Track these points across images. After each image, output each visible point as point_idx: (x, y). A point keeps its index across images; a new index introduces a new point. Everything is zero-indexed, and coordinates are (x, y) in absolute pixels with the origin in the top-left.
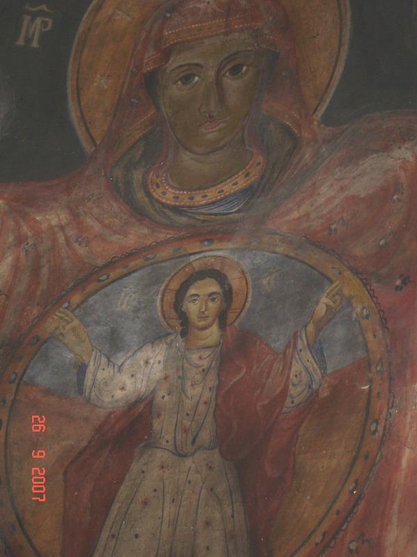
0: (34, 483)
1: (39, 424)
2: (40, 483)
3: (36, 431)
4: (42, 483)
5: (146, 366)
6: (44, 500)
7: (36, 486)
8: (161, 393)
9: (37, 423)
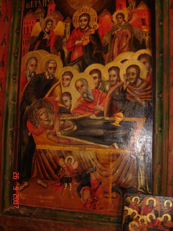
0: (14, 200)
1: (16, 176)
2: (15, 202)
3: (15, 179)
4: (17, 200)
5: (60, 82)
6: (18, 207)
7: (17, 200)
8: (118, 103)
9: (16, 175)
